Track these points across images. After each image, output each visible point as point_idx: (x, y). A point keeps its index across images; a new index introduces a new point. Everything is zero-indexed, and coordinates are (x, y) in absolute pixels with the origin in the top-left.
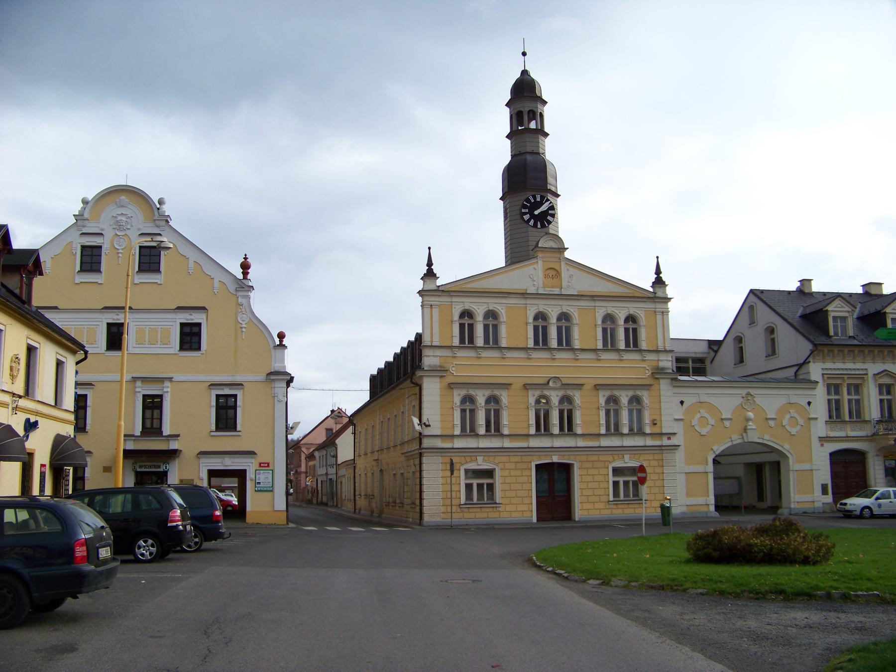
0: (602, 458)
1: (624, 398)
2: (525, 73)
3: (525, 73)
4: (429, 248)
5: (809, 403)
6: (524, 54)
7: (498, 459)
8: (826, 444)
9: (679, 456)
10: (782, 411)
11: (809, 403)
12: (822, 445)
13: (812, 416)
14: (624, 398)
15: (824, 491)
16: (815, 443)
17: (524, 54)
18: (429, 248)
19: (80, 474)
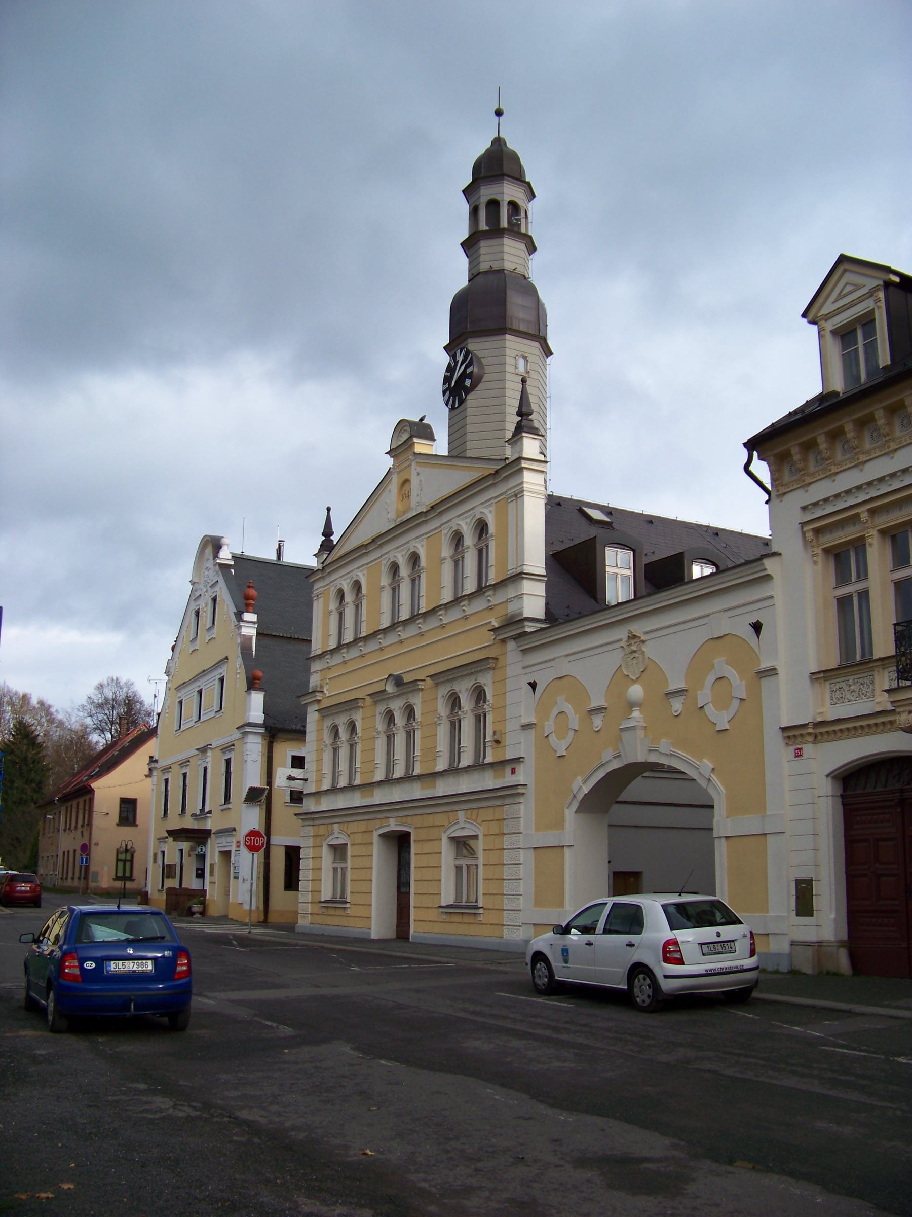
0: (430, 820)
1: (464, 689)
2: (498, 142)
3: (498, 142)
4: (329, 509)
5: (757, 627)
6: (499, 113)
7: (353, 827)
8: (808, 749)
9: (525, 811)
10: (698, 665)
11: (757, 627)
12: (799, 753)
13: (765, 665)
14: (464, 689)
15: (804, 903)
16: (773, 742)
17: (499, 113)
18: (329, 509)
19: (403, 890)
